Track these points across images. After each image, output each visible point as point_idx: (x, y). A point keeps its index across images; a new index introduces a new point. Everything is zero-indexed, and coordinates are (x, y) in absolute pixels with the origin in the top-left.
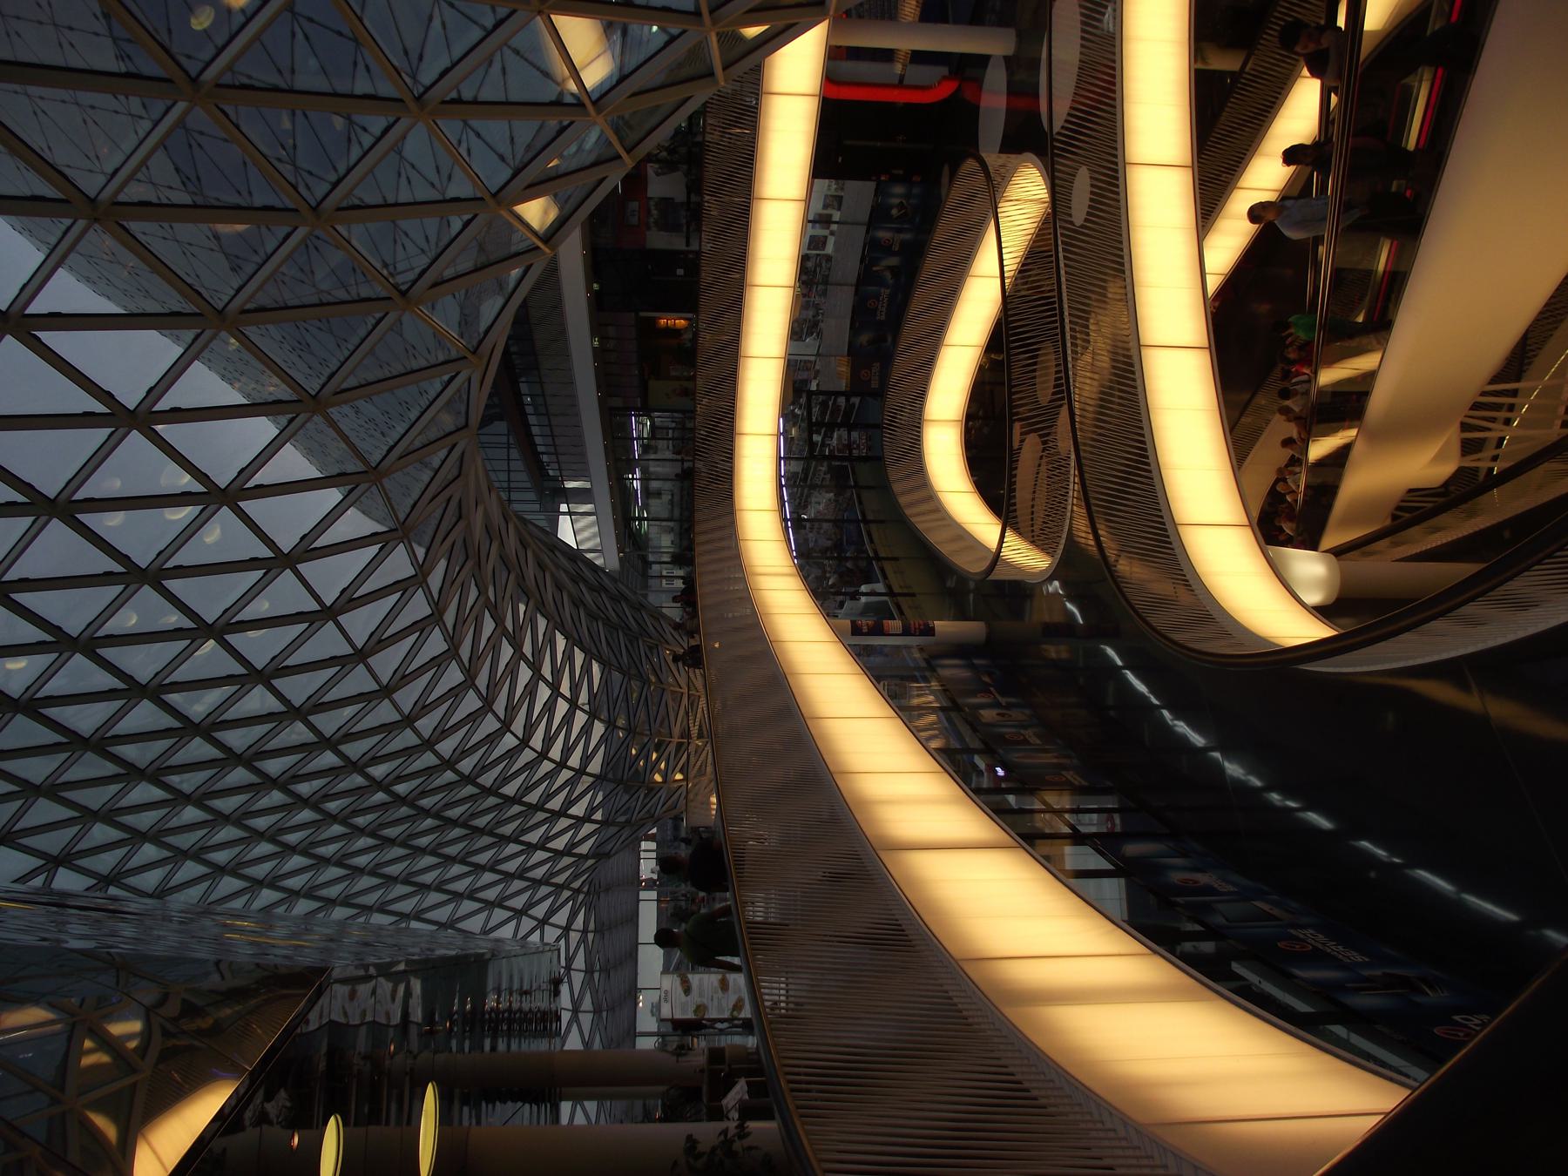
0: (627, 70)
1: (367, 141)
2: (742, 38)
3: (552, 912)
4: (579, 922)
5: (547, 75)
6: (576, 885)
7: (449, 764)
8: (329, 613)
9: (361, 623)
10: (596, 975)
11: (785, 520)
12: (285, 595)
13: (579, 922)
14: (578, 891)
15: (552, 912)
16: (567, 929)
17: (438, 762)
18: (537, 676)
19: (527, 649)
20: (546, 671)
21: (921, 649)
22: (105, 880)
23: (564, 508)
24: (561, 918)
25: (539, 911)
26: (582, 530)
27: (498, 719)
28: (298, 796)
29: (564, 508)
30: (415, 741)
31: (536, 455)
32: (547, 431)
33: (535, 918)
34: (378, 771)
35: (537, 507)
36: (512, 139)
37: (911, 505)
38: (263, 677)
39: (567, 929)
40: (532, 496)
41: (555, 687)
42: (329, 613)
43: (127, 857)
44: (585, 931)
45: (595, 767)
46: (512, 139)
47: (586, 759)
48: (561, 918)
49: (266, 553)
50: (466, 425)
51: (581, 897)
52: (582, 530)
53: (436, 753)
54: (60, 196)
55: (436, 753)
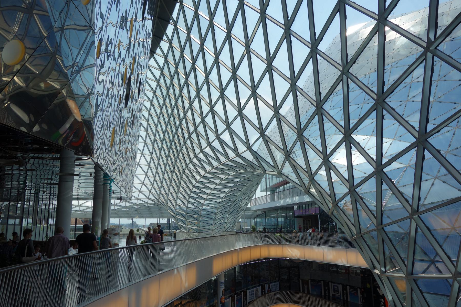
0: (388, 233)
1: (417, 257)
4: (150, 201)
7: (187, 166)
8: (218, 137)
9: (226, 137)
10: (136, 207)
11: (259, 260)
12: (221, 127)
14: (159, 201)
21: (217, 302)
23: (269, 193)
24: (151, 197)
25: (153, 191)
26: (263, 199)
29: (269, 193)
31: (103, 194)
32: (291, 187)
34: (188, 142)
35: (268, 186)
36: (405, 186)
37: (257, 302)
40: (271, 185)
42: (218, 137)
43: (314, 148)
44: (148, 203)
46: (405, 186)
48: (151, 197)
49: (230, 121)
52: (263, 199)
54: (348, 61)
55: (193, 158)
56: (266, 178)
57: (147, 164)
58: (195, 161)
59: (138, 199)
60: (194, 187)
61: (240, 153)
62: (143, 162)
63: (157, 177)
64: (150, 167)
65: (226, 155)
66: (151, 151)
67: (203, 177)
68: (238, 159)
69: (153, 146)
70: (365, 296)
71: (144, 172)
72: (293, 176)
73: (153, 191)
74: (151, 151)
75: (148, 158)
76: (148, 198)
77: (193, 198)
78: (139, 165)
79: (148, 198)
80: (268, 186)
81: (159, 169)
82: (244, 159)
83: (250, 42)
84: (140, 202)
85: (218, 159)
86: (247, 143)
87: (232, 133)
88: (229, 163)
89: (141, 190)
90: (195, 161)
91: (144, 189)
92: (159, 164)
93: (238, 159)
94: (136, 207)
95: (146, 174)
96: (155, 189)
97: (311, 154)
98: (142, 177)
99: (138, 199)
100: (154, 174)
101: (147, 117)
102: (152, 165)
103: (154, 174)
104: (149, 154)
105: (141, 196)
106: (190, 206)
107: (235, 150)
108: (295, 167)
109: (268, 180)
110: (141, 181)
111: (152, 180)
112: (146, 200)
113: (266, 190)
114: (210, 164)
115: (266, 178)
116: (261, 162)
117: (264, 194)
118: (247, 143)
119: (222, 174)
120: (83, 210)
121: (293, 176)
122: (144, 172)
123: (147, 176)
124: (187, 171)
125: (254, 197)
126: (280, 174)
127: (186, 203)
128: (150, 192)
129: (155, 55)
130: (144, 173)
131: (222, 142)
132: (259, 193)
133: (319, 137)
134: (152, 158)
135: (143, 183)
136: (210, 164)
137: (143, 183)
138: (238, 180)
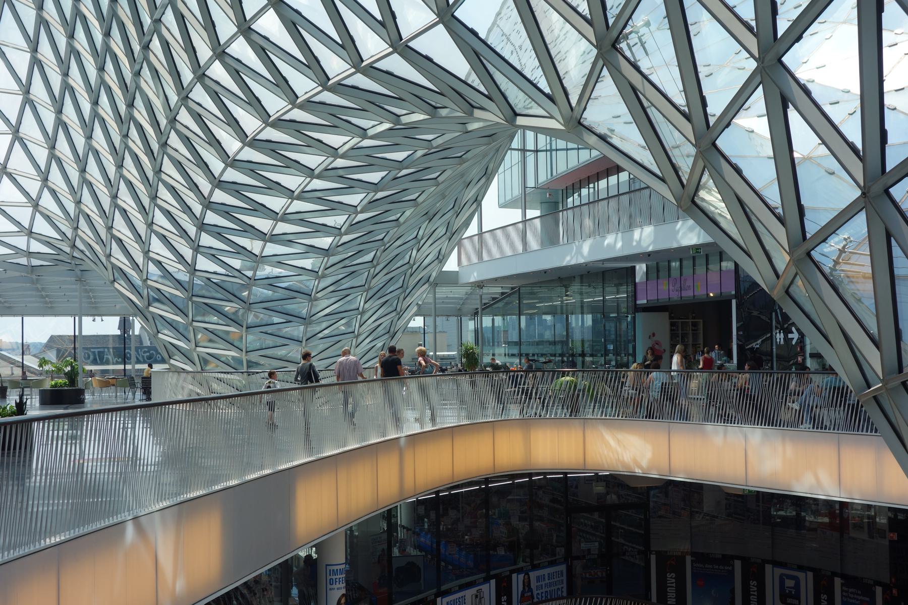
4: (36, 247)
11: (487, 481)
14: (74, 246)
24: (42, 227)
29: (532, 213)
35: (531, 183)
40: (542, 178)
44: (30, 254)
48: (42, 227)
51: (68, 250)
52: (508, 237)
56: (524, 150)
60: (219, 183)
61: (405, 35)
63: (62, 145)
68: (398, 65)
72: (630, 139)
73: (47, 201)
76: (30, 233)
77: (217, 232)
79: (30, 233)
80: (531, 183)
90: (218, 71)
93: (398, 65)
96: (53, 193)
100: (50, 130)
102: (38, 90)
103: (50, 130)
106: (203, 263)
108: (637, 96)
109: (531, 158)
111: (41, 155)
112: (21, 242)
113: (523, 202)
115: (524, 150)
116: (498, 77)
117: (515, 215)
121: (630, 139)
124: (184, 117)
125: (472, 230)
126: (576, 126)
127: (188, 253)
128: (36, 205)
132: (496, 212)
134: (36, 62)
136: (282, 84)
138: (400, 156)
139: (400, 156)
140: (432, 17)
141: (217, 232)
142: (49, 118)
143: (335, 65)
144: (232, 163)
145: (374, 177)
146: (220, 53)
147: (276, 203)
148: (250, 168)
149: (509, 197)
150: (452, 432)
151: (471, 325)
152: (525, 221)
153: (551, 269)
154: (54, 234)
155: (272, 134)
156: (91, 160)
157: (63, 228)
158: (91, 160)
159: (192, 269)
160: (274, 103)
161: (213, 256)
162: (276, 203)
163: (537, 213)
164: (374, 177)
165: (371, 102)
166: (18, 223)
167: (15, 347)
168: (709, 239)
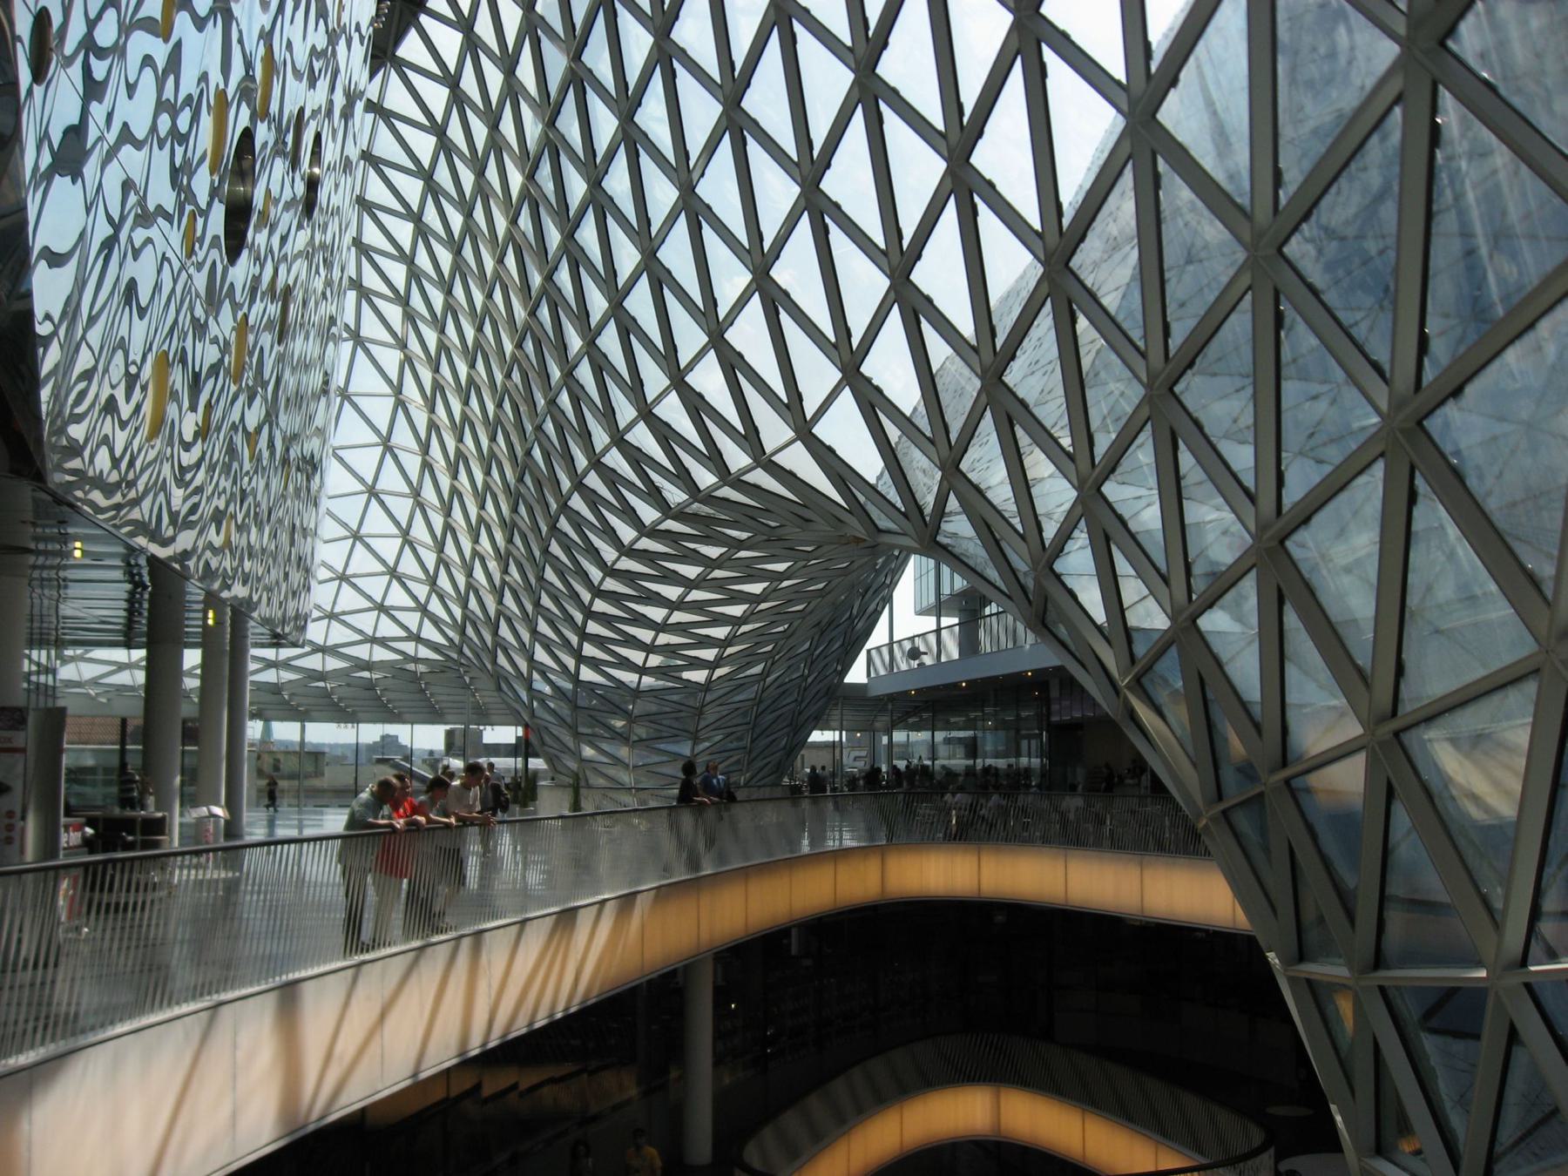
2: (1249, 881)
3: (436, 621)
4: (424, 653)
5: (643, 926)
6: (466, 650)
9: (709, 380)
13: (424, 653)
14: (461, 652)
15: (436, 621)
16: (417, 638)
17: (622, 425)
18: (690, 585)
19: (718, 574)
20: (696, 595)
22: (357, 284)
24: (430, 632)
25: (435, 606)
27: (615, 562)
28: (537, 305)
29: (946, 621)
30: (598, 448)
33: (428, 601)
38: (617, 310)
39: (417, 638)
41: (679, 605)
42: (678, 380)
44: (416, 660)
45: (587, 674)
47: (594, 664)
48: (430, 632)
50: (880, 531)
51: (455, 656)
53: (606, 449)
55: (606, 449)
57: (388, 390)
58: (593, 481)
59: (373, 640)
60: (598, 593)
61: (768, 450)
62: (365, 379)
63: (450, 549)
64: (401, 403)
65: (714, 459)
66: (423, 436)
67: (653, 532)
68: (760, 477)
69: (432, 410)
70: (210, 622)
71: (397, 524)
73: (435, 606)
74: (423, 436)
75: (413, 464)
77: (599, 641)
78: (345, 395)
80: (946, 590)
81: (450, 549)
82: (787, 476)
83: (695, 176)
84: (381, 654)
85: (683, 478)
86: (792, 407)
87: (733, 364)
88: (727, 492)
89: (363, 531)
90: (593, 481)
91: (398, 597)
92: (448, 527)
93: (760, 477)
94: (366, 674)
95: (405, 534)
96: (441, 598)
97: (1039, 465)
98: (365, 462)
99: (373, 640)
100: (439, 534)
101: (401, 286)
102: (429, 493)
103: (439, 534)
104: (416, 447)
105: (387, 629)
106: (587, 674)
107: (750, 438)
110: (383, 562)
111: (430, 559)
112: (409, 648)
113: (938, 609)
114: (654, 496)
117: (929, 623)
118: (792, 407)
119: (707, 539)
120: (94, 682)
122: (397, 524)
123: (411, 545)
124: (564, 524)
127: (570, 662)
129: (424, 19)
130: (395, 531)
131: (696, 405)
133: (995, 434)
134: (427, 466)
135: (373, 492)
136: (654, 496)
137: (373, 492)
138: (781, 567)
139: (781, 567)
140: (791, 434)
141: (599, 641)
142: (438, 521)
143: (705, 478)
144: (610, 571)
145: (756, 588)
146: (596, 464)
147: (656, 614)
148: (627, 577)
149: (925, 604)
150: (843, 854)
151: (885, 740)
152: (938, 631)
153: (1006, 676)
154: (442, 640)
155: (645, 543)
156: (477, 564)
157: (451, 634)
158: (477, 564)
159: (575, 678)
160: (648, 514)
161: (594, 664)
162: (656, 614)
163: (956, 620)
164: (756, 588)
165: (742, 516)
166: (406, 628)
167: (345, 757)
168: (1056, 662)
